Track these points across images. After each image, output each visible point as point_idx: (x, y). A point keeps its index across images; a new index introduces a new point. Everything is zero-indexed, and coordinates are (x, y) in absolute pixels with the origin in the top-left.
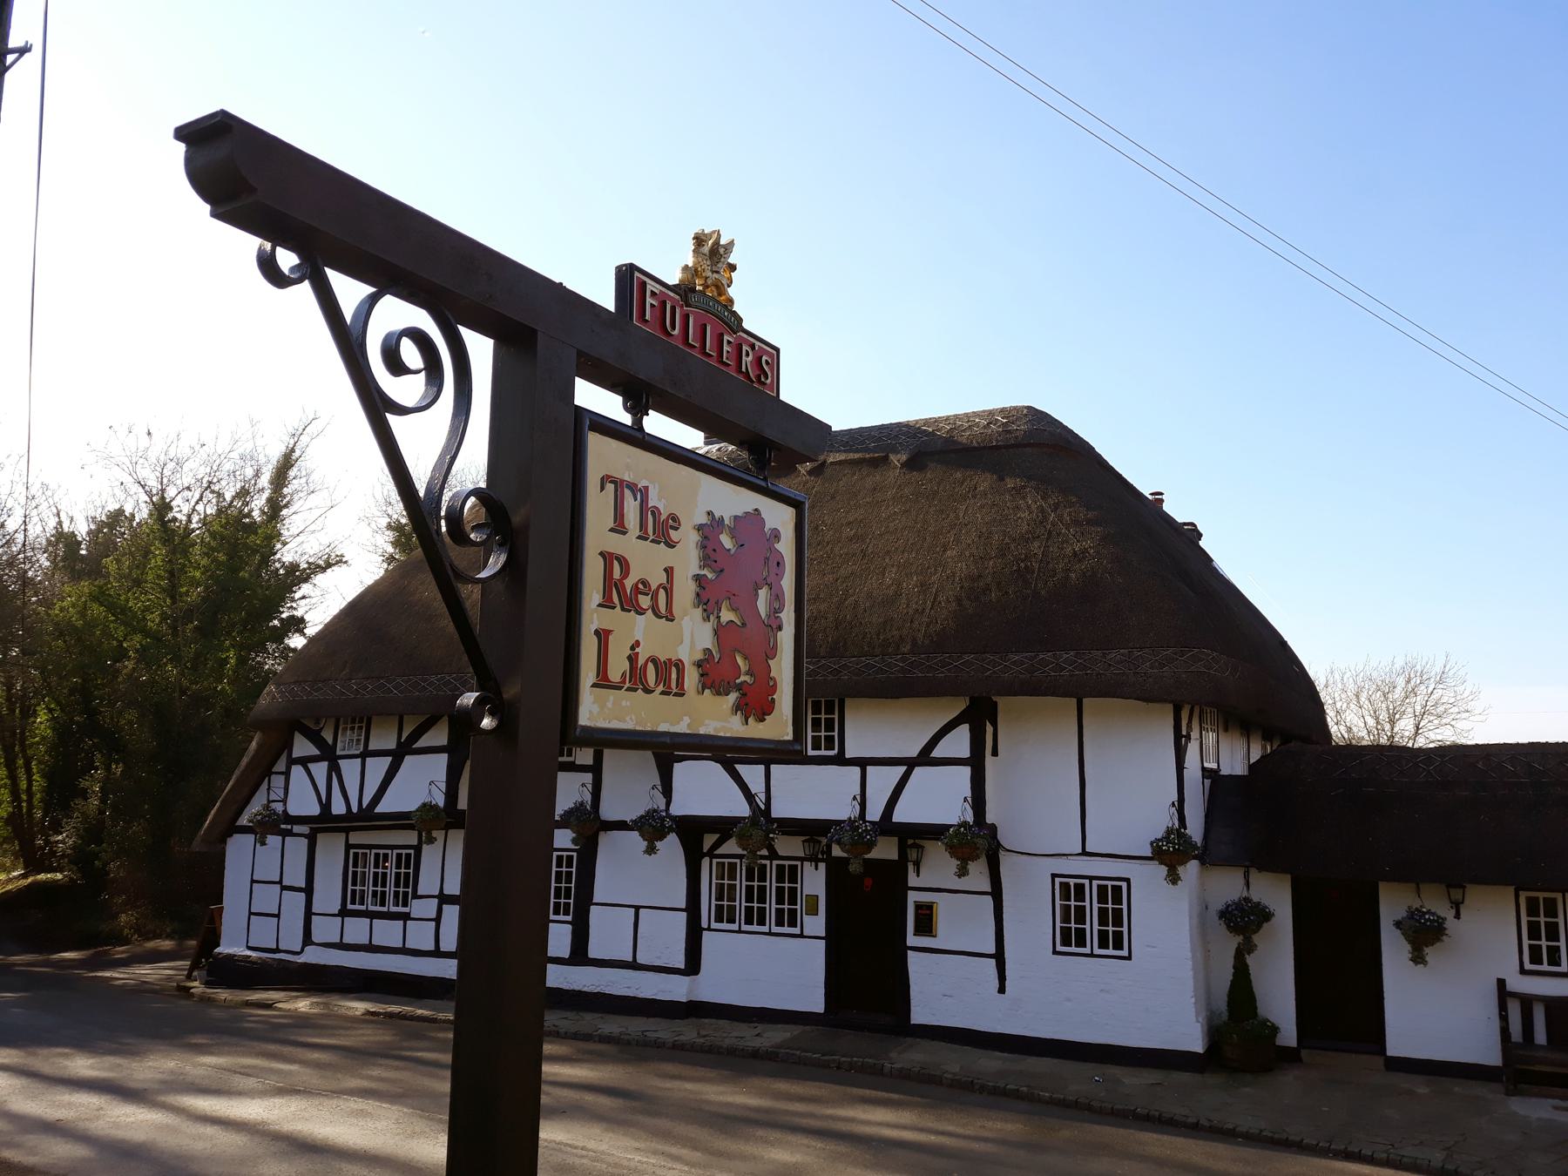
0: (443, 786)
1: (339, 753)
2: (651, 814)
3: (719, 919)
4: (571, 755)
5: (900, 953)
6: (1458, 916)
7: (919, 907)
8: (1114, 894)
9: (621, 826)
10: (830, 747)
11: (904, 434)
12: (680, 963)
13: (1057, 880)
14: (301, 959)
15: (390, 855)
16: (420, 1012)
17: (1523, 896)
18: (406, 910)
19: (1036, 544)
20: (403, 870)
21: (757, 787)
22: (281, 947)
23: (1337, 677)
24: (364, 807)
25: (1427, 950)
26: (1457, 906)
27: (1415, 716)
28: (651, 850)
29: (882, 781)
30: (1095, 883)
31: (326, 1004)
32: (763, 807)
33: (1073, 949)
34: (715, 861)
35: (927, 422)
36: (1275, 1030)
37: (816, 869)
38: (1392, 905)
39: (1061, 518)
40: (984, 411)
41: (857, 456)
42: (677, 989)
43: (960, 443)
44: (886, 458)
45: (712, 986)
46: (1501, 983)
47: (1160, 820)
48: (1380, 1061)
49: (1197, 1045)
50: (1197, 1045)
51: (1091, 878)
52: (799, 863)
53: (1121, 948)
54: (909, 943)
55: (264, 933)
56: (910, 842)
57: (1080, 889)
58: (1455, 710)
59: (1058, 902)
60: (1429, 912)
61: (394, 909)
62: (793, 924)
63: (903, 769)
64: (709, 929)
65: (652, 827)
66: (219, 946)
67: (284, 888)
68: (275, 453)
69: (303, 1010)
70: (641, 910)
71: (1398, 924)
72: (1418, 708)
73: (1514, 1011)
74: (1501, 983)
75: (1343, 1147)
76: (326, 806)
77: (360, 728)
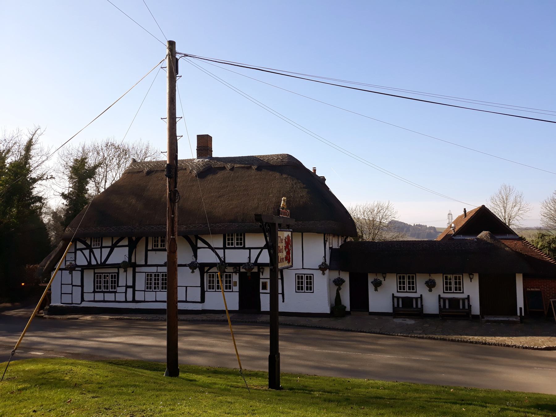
0: (128, 256)
1: (92, 247)
2: (192, 263)
3: (210, 288)
4: (164, 247)
5: (258, 294)
6: (384, 280)
7: (263, 283)
8: (310, 278)
9: (185, 266)
10: (241, 244)
11: (255, 160)
12: (199, 300)
13: (297, 275)
14: (81, 305)
15: (109, 276)
16: (126, 317)
17: (398, 275)
18: (115, 290)
19: (292, 194)
20: (113, 279)
21: (221, 255)
22: (73, 302)
23: (358, 208)
24: (102, 262)
25: (378, 288)
26: (384, 278)
27: (380, 219)
28: (193, 272)
29: (255, 253)
30: (305, 275)
31: (96, 317)
32: (223, 260)
33: (300, 291)
34: (208, 274)
35: (261, 156)
36: (345, 307)
37: (236, 275)
38: (371, 278)
39: (297, 186)
40: (276, 155)
41: (243, 165)
42: (199, 307)
43: (271, 164)
44: (251, 167)
45: (208, 306)
46: (393, 294)
47: (321, 260)
48: (368, 313)
49: (328, 311)
50: (328, 311)
51: (304, 274)
52: (231, 274)
53: (303, 290)
54: (260, 292)
55: (67, 299)
56: (261, 267)
57: (302, 277)
58: (391, 217)
59: (297, 280)
60: (378, 279)
61: (111, 290)
62: (230, 289)
63: (260, 250)
64: (207, 291)
65: (193, 266)
66: (51, 303)
67: (73, 286)
68: (24, 141)
69: (89, 319)
70: (188, 287)
71: (372, 282)
72: (381, 217)
73: (396, 300)
74: (393, 294)
75: (360, 330)
76: (89, 262)
77: (99, 241)
